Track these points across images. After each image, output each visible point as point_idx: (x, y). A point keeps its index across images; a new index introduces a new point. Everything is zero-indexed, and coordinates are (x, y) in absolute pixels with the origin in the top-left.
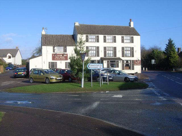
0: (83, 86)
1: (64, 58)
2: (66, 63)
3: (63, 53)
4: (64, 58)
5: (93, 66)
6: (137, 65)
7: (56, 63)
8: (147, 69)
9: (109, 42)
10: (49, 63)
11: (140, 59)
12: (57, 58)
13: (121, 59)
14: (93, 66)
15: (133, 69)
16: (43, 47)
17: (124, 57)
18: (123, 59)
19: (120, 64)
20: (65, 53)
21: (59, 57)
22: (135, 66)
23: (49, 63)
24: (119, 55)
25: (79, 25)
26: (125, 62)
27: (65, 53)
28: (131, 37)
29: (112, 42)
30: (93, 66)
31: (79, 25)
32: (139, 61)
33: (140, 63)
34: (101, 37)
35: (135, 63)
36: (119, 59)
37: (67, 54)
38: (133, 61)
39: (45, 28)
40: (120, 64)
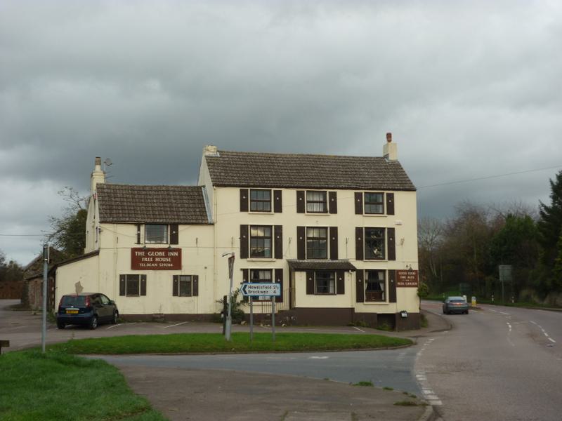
0: (554, 341)
1: (168, 262)
2: (175, 277)
3: (166, 246)
4: (168, 262)
5: (256, 290)
6: (405, 286)
7: (144, 277)
8: (474, 300)
9: (315, 210)
10: (122, 277)
11: (415, 267)
12: (146, 262)
13: (354, 269)
14: (255, 288)
15: (393, 299)
16: (354, 273)
17: (362, 260)
18: (360, 265)
19: (350, 281)
20: (173, 246)
21: (154, 257)
22: (399, 291)
23: (122, 277)
24: (347, 251)
25: (219, 155)
26: (366, 277)
27: (173, 246)
28: (387, 194)
29: (269, 192)
30: (255, 288)
31: (219, 155)
32: (414, 273)
33: (415, 280)
34: (289, 197)
35: (400, 280)
36: (348, 267)
37: (179, 251)
38: (392, 272)
39: (103, 160)
40: (350, 281)
